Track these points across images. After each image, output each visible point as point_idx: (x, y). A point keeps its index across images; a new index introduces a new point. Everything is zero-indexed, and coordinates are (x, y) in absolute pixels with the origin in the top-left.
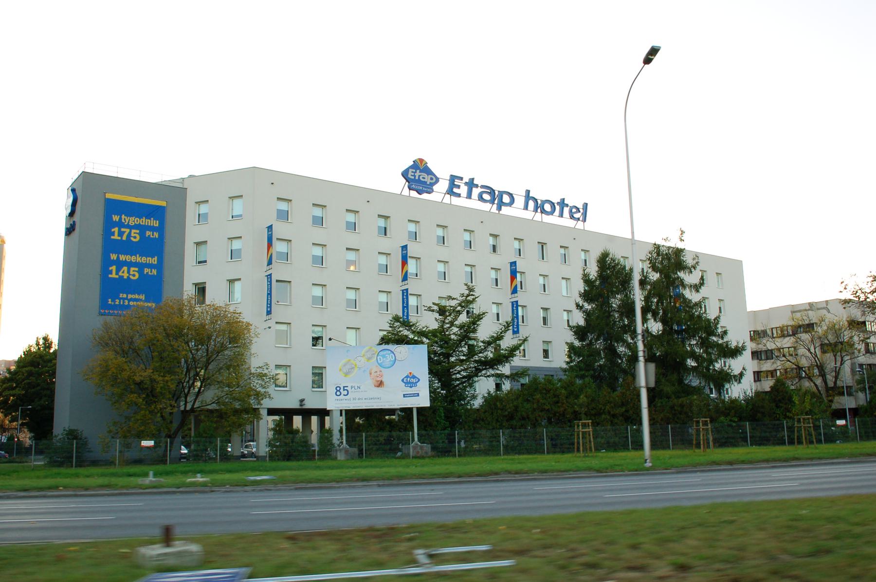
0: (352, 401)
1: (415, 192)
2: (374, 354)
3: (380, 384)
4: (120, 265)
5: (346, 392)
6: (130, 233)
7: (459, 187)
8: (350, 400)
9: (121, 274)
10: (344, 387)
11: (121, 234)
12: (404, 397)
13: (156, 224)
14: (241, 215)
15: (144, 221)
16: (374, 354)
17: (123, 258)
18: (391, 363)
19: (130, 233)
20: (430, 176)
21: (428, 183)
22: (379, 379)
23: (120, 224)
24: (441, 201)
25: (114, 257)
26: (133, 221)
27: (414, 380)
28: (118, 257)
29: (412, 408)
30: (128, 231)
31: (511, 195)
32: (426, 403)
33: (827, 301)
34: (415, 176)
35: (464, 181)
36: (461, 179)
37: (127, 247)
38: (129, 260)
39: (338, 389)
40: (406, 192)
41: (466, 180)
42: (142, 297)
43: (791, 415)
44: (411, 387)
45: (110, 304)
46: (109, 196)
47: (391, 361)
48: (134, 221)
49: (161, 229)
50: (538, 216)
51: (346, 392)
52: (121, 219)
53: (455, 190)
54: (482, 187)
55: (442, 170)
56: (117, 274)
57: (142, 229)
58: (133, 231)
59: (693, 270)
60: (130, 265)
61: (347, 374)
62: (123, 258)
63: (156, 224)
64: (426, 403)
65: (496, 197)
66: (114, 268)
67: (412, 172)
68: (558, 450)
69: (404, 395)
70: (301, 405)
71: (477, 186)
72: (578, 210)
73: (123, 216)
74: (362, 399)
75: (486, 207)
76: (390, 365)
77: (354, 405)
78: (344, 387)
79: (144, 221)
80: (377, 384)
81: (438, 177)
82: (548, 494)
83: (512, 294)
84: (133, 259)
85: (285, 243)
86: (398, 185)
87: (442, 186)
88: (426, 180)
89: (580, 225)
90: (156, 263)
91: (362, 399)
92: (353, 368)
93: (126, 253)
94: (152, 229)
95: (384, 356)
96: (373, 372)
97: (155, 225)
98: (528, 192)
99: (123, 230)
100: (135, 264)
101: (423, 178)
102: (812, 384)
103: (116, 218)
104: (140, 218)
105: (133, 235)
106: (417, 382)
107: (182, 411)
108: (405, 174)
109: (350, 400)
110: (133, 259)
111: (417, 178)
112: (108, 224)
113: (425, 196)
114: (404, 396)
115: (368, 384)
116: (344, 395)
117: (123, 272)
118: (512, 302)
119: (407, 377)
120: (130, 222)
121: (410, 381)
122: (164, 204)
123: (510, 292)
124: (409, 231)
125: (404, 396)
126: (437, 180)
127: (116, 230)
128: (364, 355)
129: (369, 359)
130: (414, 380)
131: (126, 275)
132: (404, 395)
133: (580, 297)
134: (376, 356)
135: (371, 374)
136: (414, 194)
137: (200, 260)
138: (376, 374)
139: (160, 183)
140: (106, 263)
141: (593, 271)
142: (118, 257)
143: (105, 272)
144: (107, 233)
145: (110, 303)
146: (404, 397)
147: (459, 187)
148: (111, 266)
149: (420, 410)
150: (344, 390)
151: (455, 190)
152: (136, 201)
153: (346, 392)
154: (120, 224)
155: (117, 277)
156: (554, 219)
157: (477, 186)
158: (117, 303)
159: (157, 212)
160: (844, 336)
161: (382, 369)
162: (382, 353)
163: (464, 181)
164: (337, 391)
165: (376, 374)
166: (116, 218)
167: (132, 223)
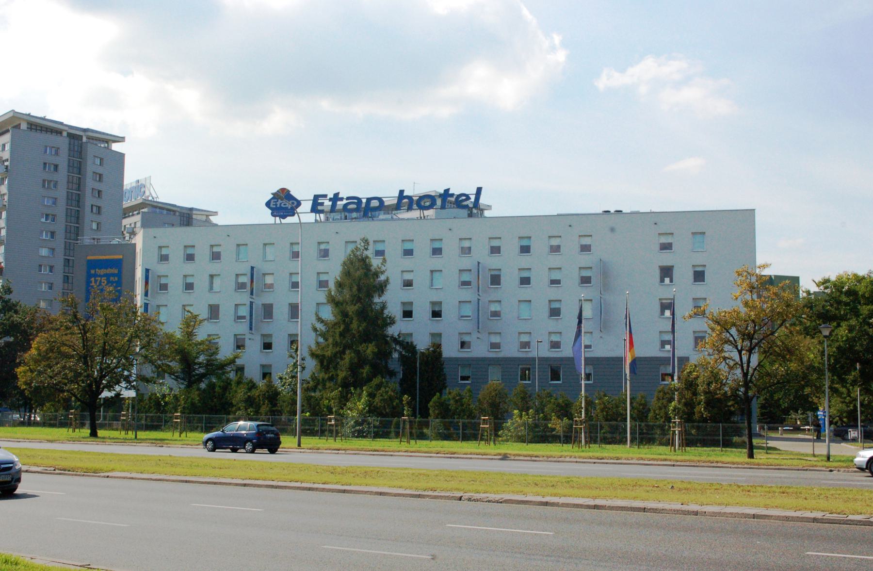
6: (101, 281)
7: (322, 204)
13: (116, 271)
19: (101, 281)
21: (289, 208)
23: (95, 276)
24: (274, 223)
26: (102, 272)
30: (100, 278)
33: (191, 209)
34: (276, 205)
35: (328, 198)
36: (325, 196)
41: (331, 196)
43: (234, 388)
52: (95, 271)
53: (320, 208)
54: (348, 198)
55: (303, 193)
58: (103, 278)
67: (274, 202)
71: (342, 199)
73: (97, 270)
81: (299, 199)
85: (558, 335)
86: (266, 217)
87: (306, 206)
88: (287, 206)
93: (585, 411)
94: (113, 275)
99: (97, 278)
101: (284, 205)
103: (93, 272)
104: (107, 268)
105: (103, 281)
108: (268, 204)
111: (278, 206)
113: (289, 220)
119: (276, 196)
122: (121, 257)
126: (299, 203)
127: (93, 279)
133: (241, 286)
137: (464, 375)
151: (320, 208)
157: (342, 199)
163: (328, 198)
166: (93, 272)
167: (102, 274)
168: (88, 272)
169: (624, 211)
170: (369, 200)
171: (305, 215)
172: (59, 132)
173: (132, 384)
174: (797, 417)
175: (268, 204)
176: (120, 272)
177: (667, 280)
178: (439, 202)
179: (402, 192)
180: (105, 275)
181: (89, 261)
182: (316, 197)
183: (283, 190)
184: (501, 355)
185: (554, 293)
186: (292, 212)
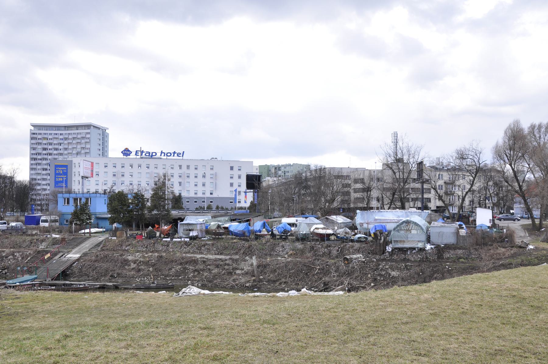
4: (58, 177)
11: (58, 171)
13: (66, 169)
15: (63, 168)
17: (59, 176)
23: (58, 170)
25: (57, 176)
26: (61, 168)
27: (128, 153)
31: (155, 153)
33: (341, 168)
37: (60, 174)
40: (123, 157)
46: (55, 164)
49: (67, 170)
53: (137, 154)
55: (133, 149)
57: (63, 170)
60: (60, 178)
62: (59, 176)
63: (66, 169)
66: (57, 179)
68: (337, 186)
71: (144, 152)
72: (180, 154)
79: (63, 168)
84: (61, 176)
86: (121, 156)
87: (134, 153)
94: (65, 170)
98: (162, 151)
100: (62, 177)
102: (533, 176)
103: (57, 168)
108: (122, 152)
110: (61, 176)
112: (56, 170)
119: (125, 150)
122: (67, 164)
126: (131, 152)
130: (128, 153)
136: (125, 157)
140: (55, 178)
143: (55, 179)
144: (55, 172)
147: (138, 153)
151: (137, 154)
154: (58, 170)
156: (171, 157)
157: (144, 152)
159: (66, 166)
160: (44, 246)
166: (57, 168)
168: (67, 171)
169: (219, 159)
170: (152, 153)
171: (133, 156)
172: (99, 128)
173: (385, 272)
174: (355, 225)
175: (122, 152)
176: (67, 169)
177: (140, 167)
178: (172, 154)
179: (162, 151)
180: (61, 170)
181: (55, 165)
182: (137, 151)
183: (127, 148)
184: (197, 196)
185: (115, 170)
186: (129, 155)
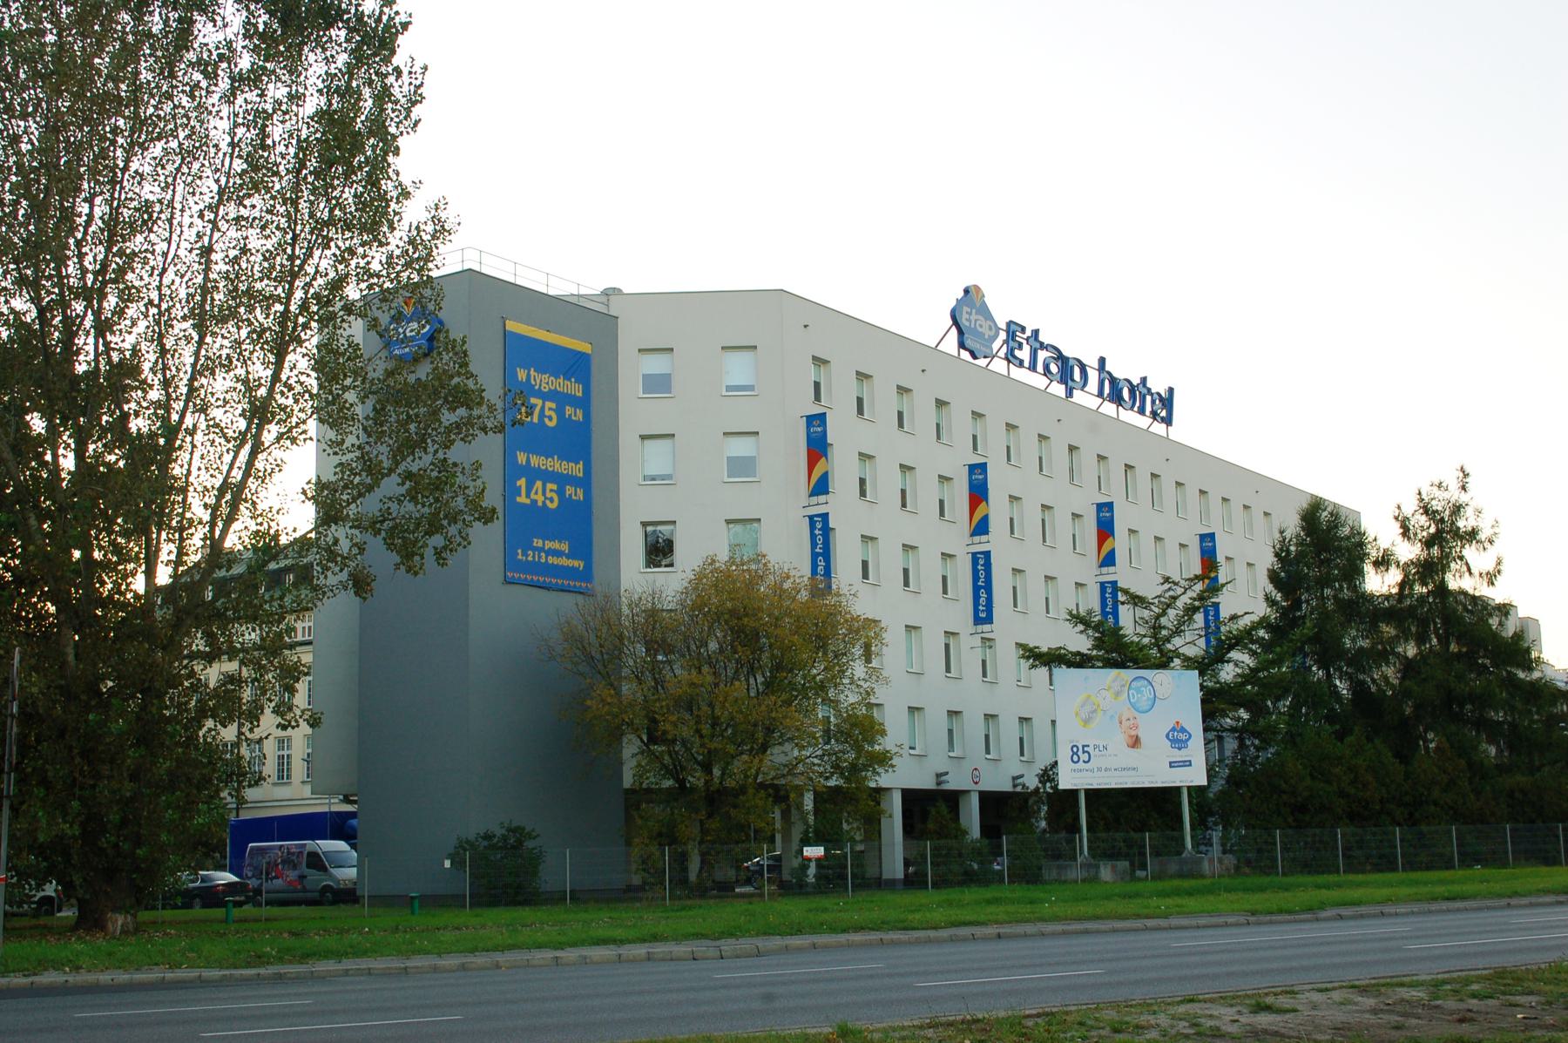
0: (1096, 774)
1: (967, 353)
2: (1124, 686)
3: (1135, 742)
4: (533, 475)
5: (1085, 757)
8: (1092, 771)
9: (533, 496)
10: (1083, 746)
12: (1171, 767)
14: (753, 386)
16: (1124, 686)
17: (536, 461)
18: (1150, 703)
19: (543, 408)
20: (989, 323)
22: (1133, 733)
28: (528, 460)
29: (1178, 789)
30: (539, 402)
32: (1202, 781)
38: (544, 467)
39: (1075, 749)
42: (565, 547)
44: (1180, 749)
45: (520, 560)
46: (512, 326)
47: (1148, 699)
48: (548, 383)
50: (1109, 408)
51: (1086, 754)
56: (528, 496)
59: (1487, 545)
61: (1086, 721)
64: (1202, 781)
65: (1066, 369)
69: (1170, 763)
70: (939, 784)
74: (1110, 770)
75: (1038, 381)
76: (1148, 708)
77: (1100, 781)
78: (1083, 746)
80: (1131, 742)
82: (1381, 940)
83: (972, 535)
89: (1159, 428)
90: (581, 475)
91: (1110, 770)
92: (1095, 711)
95: (1138, 690)
96: (1124, 719)
97: (577, 394)
101: (981, 326)
105: (547, 413)
106: (1188, 740)
107: (627, 790)
109: (1092, 771)
114: (1171, 765)
115: (1118, 741)
116: (1084, 762)
117: (536, 493)
118: (974, 555)
119: (1173, 729)
120: (544, 385)
121: (1178, 737)
122: (584, 347)
123: (966, 530)
124: (644, 376)
125: (1171, 765)
128: (1110, 688)
129: (1118, 694)
130: (1183, 737)
131: (540, 499)
132: (1170, 763)
134: (1126, 688)
135: (1121, 723)
138: (1128, 723)
139: (574, 300)
141: (1293, 526)
142: (528, 460)
145: (520, 557)
146: (1171, 767)
148: (520, 479)
149: (1196, 792)
150: (1084, 752)
152: (518, 331)
153: (1086, 754)
155: (528, 501)
158: (530, 558)
159: (576, 365)
161: (1136, 714)
162: (1135, 684)
164: (1074, 753)
165: (1128, 723)
